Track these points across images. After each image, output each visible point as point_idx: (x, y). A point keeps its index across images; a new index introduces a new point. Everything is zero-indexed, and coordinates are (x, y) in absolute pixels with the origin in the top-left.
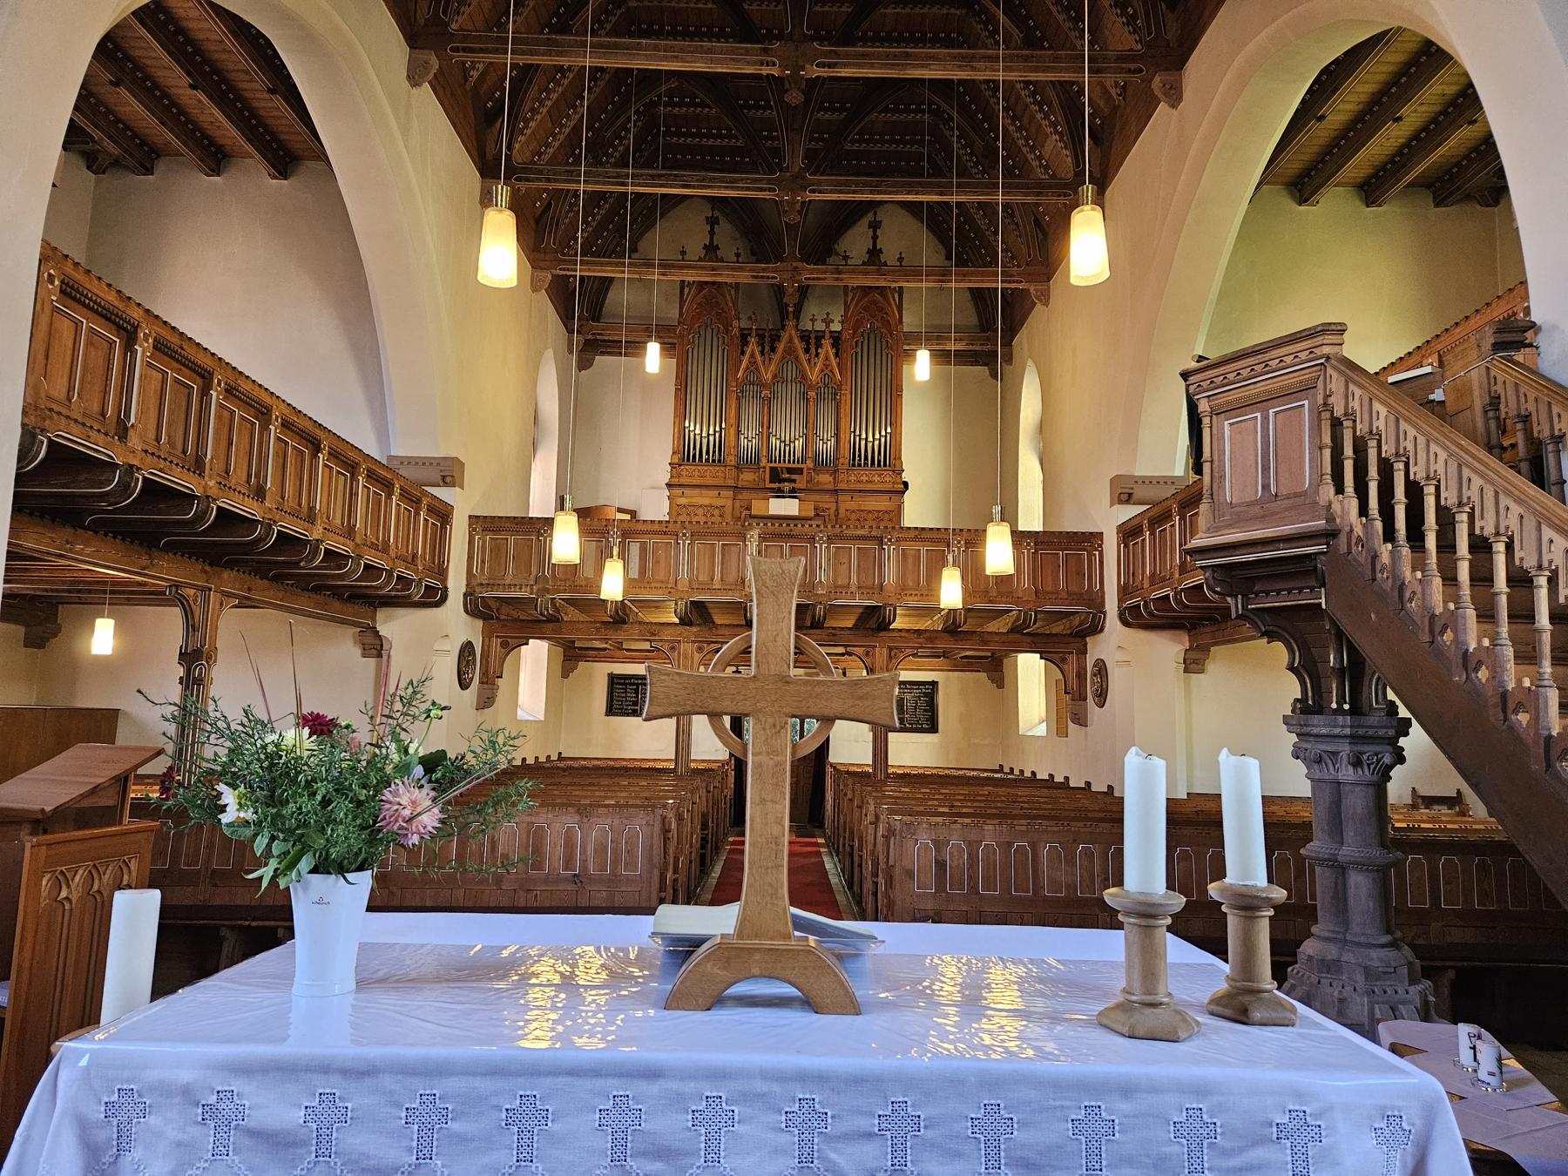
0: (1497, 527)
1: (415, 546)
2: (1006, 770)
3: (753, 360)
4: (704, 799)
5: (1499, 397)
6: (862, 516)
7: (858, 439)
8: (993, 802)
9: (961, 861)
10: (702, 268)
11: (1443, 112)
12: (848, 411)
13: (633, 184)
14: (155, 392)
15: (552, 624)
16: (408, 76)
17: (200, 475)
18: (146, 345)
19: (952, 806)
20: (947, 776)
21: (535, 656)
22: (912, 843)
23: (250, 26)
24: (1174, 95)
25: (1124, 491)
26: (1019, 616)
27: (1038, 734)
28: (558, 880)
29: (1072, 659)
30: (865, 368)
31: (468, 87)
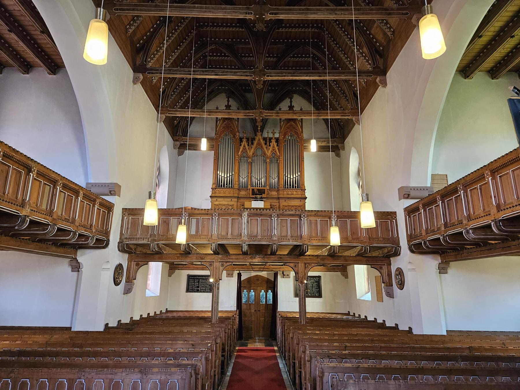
1: (75, 212)
3: (244, 148)
6: (290, 207)
12: (283, 167)
13: (194, 74)
15: (158, 255)
16: (133, 81)
25: (406, 193)
27: (366, 299)
29: (385, 268)
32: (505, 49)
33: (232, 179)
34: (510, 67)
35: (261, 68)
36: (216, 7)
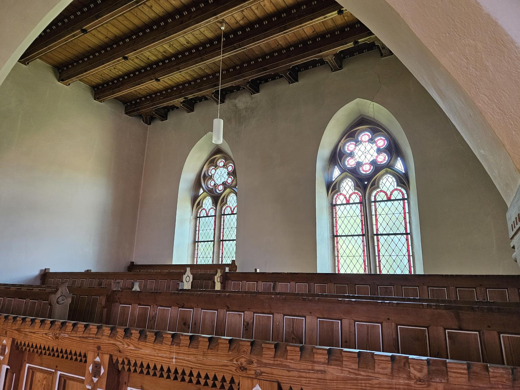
11: (145, 68)
32: (116, 70)
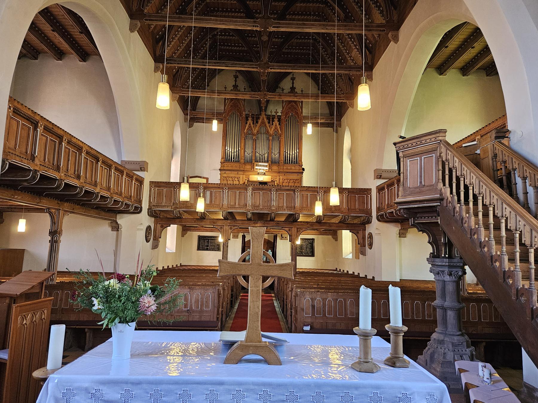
0: (490, 202)
1: (131, 192)
2: (338, 270)
3: (250, 126)
4: (232, 282)
5: (497, 154)
7: (287, 154)
8: (333, 283)
9: (320, 306)
10: (232, 93)
12: (284, 144)
14: (44, 143)
16: (130, 29)
17: (58, 172)
18: (41, 128)
19: (318, 285)
20: (317, 273)
21: (172, 231)
22: (304, 299)
23: (76, 14)
24: (396, 39)
26: (342, 217)
28: (182, 312)
29: (361, 232)
30: (289, 130)
31: (150, 31)
33: (238, 154)
34: (478, 66)
35: (265, 61)
36: (228, 20)
